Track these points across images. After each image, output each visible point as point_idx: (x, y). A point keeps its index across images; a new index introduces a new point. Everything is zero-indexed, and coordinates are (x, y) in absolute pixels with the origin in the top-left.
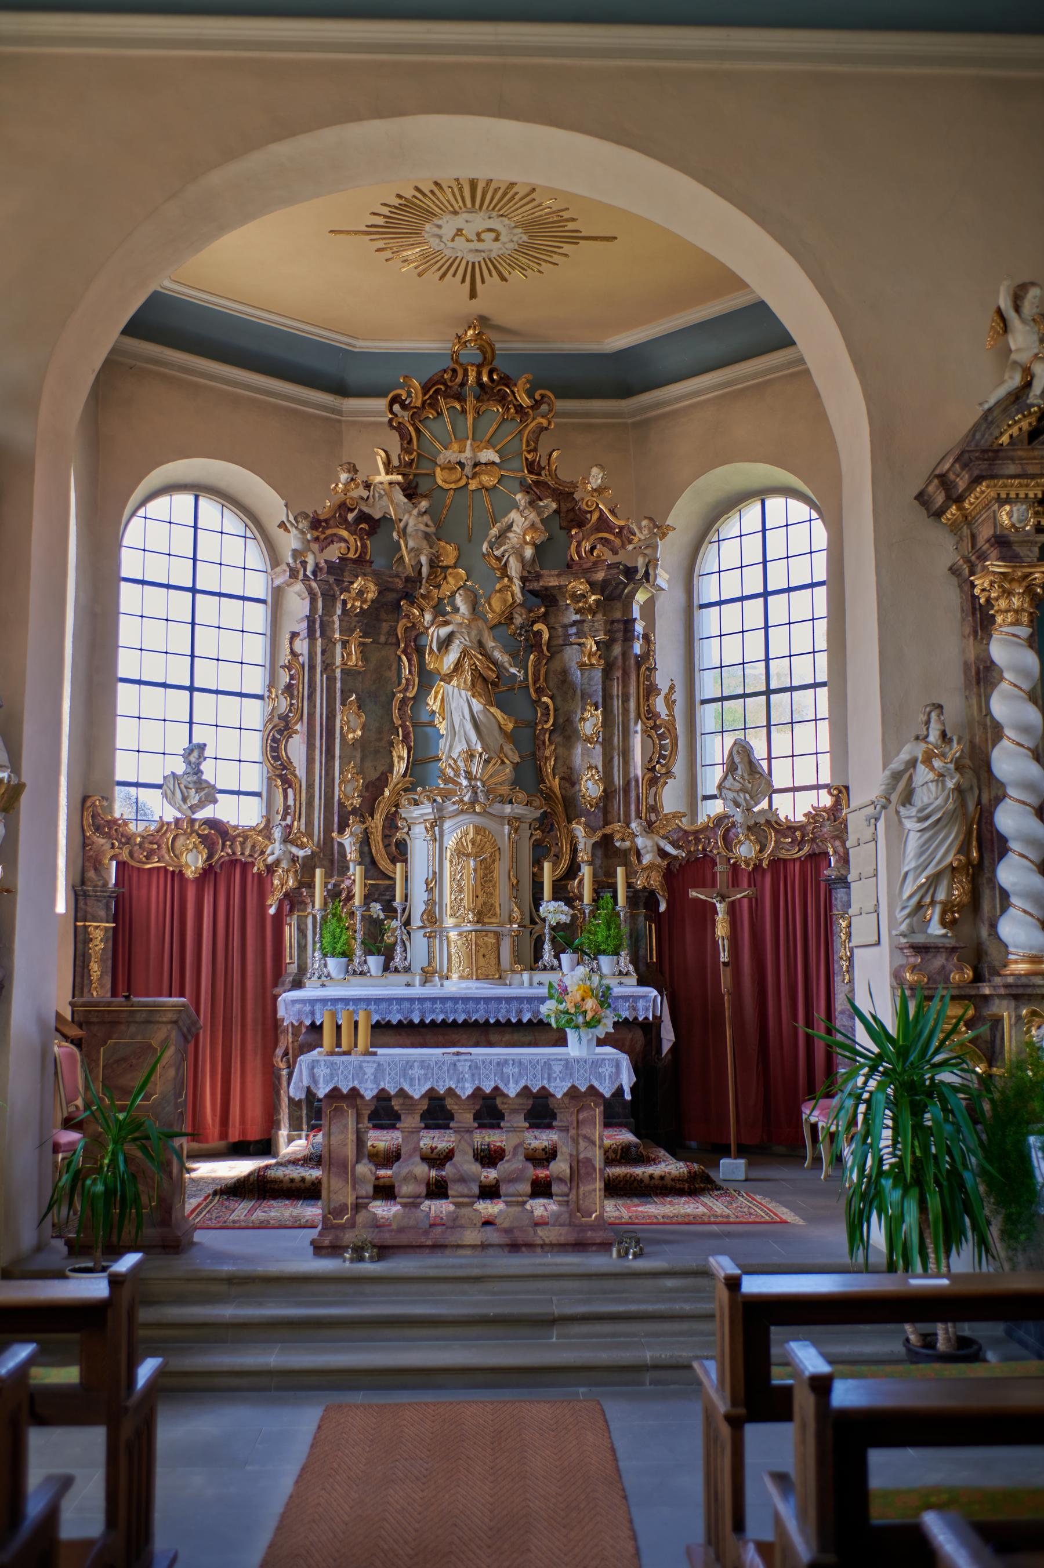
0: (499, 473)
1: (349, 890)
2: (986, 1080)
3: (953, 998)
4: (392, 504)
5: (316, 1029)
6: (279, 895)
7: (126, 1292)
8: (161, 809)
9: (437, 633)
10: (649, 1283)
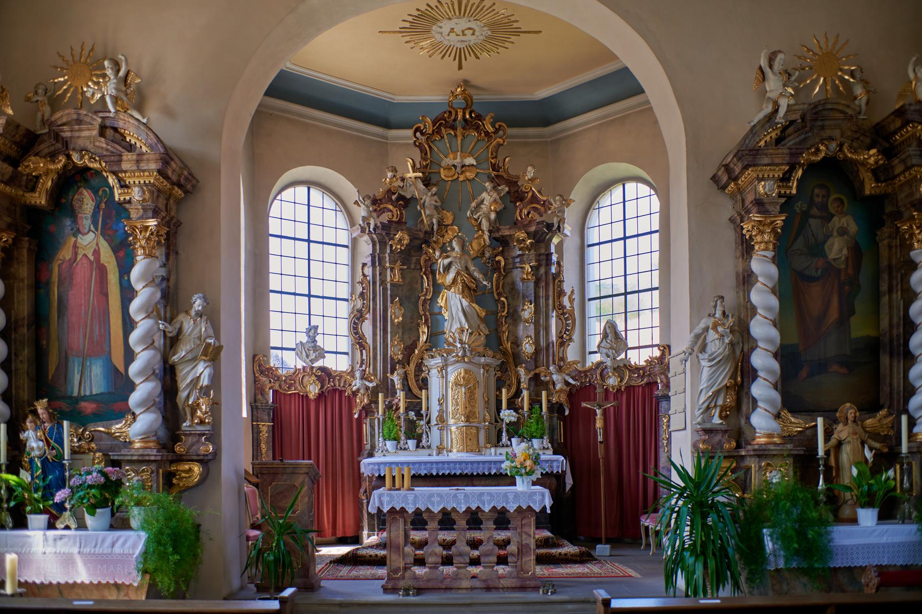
0: (475, 171)
1: (397, 405)
2: (741, 500)
3: (725, 457)
4: (417, 190)
5: (382, 478)
6: (359, 408)
7: (288, 607)
8: (292, 362)
9: (442, 262)
10: (558, 607)
